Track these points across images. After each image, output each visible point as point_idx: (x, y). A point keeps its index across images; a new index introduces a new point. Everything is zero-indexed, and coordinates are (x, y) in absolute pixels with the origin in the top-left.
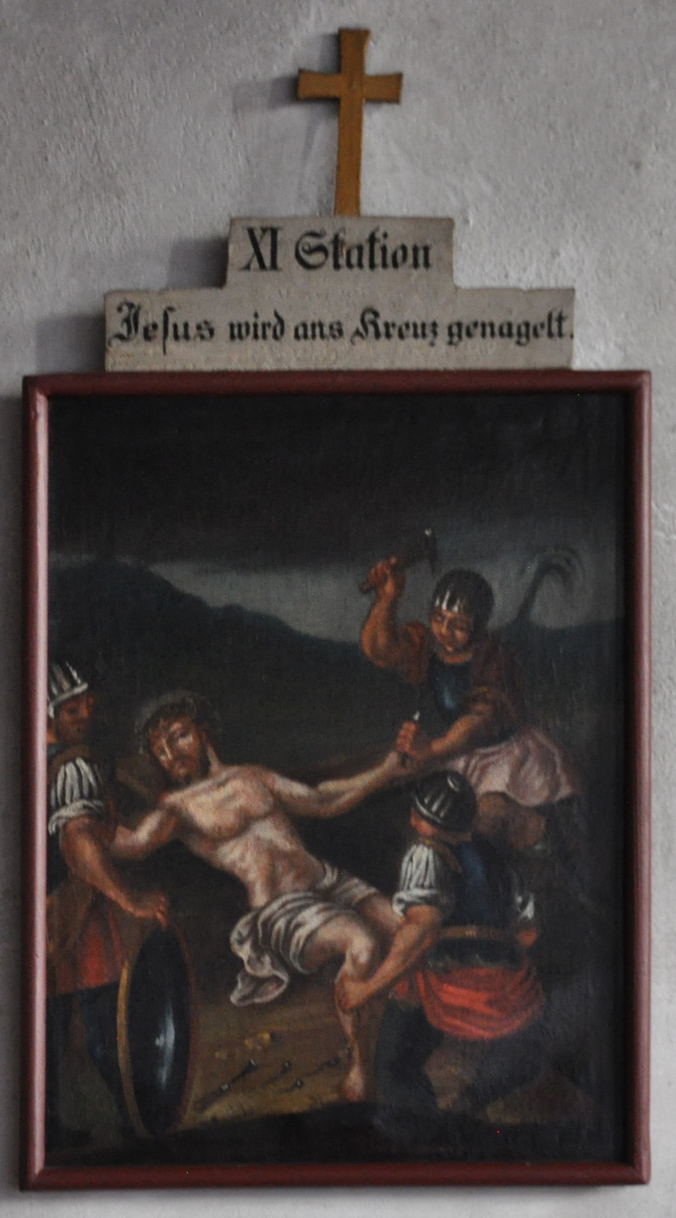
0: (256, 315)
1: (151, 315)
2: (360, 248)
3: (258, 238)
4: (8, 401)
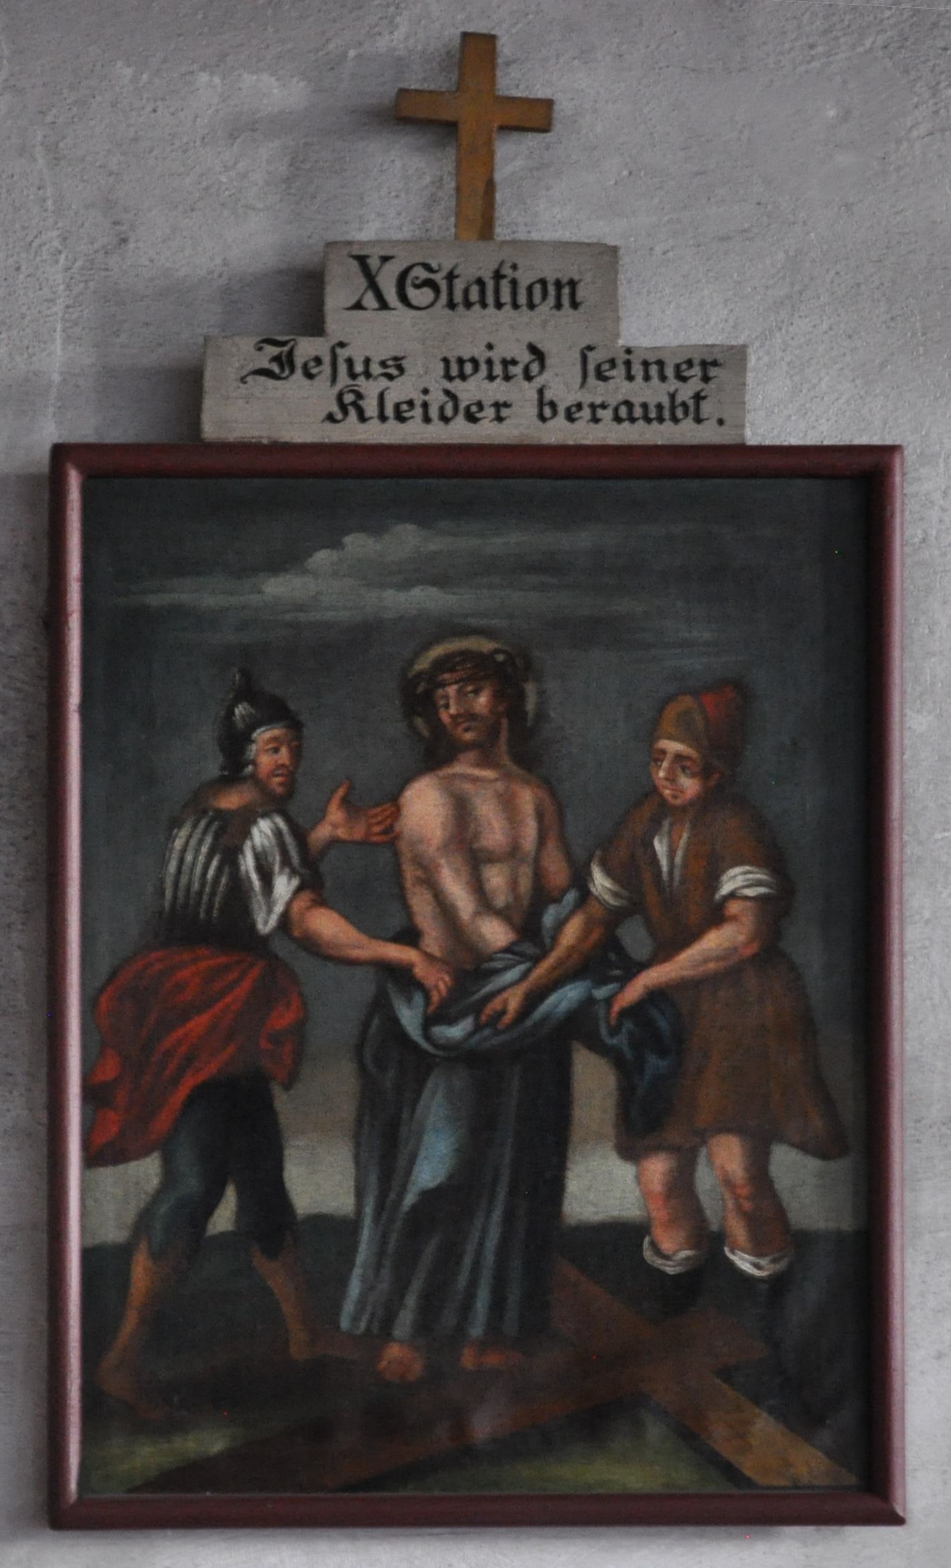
0: (490, 347)
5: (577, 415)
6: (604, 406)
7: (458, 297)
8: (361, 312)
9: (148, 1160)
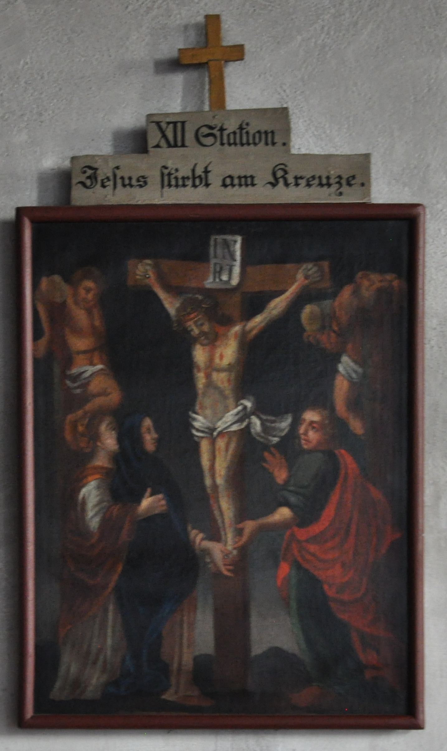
1: (105, 171)
4: (6, 223)
5: (353, 182)
7: (225, 141)
8: (185, 148)
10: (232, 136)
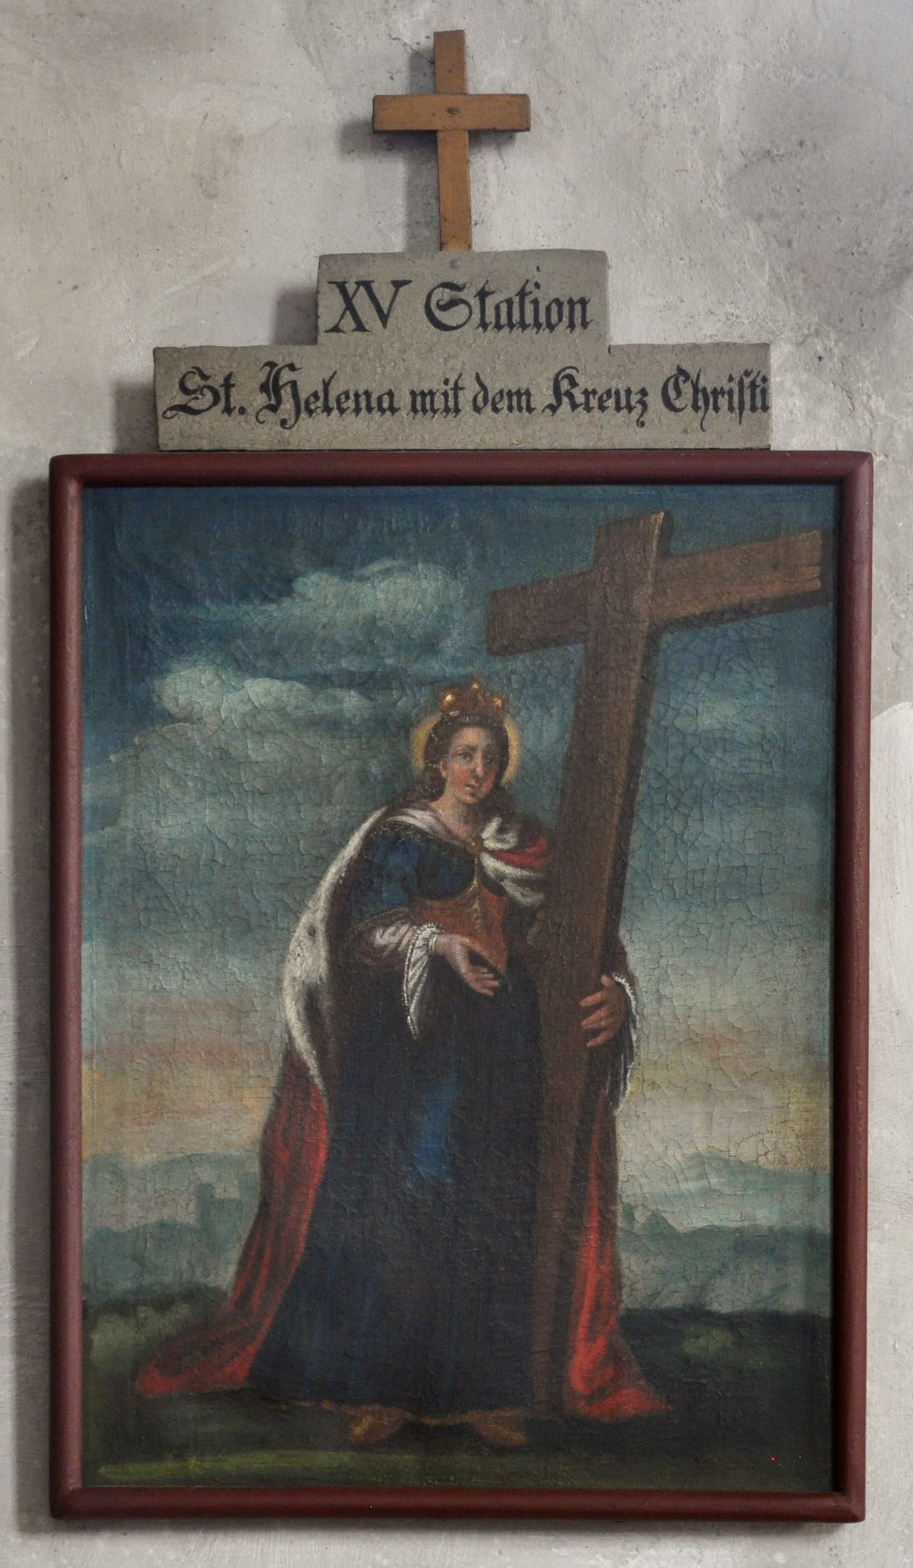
2: (509, 302)
3: (351, 293)
6: (594, 392)
9: (574, 393)
10: (504, 308)
